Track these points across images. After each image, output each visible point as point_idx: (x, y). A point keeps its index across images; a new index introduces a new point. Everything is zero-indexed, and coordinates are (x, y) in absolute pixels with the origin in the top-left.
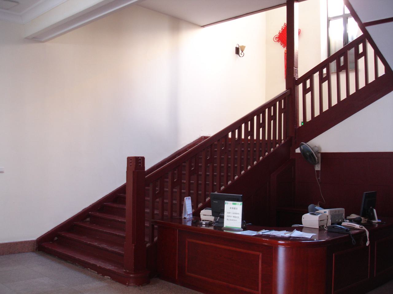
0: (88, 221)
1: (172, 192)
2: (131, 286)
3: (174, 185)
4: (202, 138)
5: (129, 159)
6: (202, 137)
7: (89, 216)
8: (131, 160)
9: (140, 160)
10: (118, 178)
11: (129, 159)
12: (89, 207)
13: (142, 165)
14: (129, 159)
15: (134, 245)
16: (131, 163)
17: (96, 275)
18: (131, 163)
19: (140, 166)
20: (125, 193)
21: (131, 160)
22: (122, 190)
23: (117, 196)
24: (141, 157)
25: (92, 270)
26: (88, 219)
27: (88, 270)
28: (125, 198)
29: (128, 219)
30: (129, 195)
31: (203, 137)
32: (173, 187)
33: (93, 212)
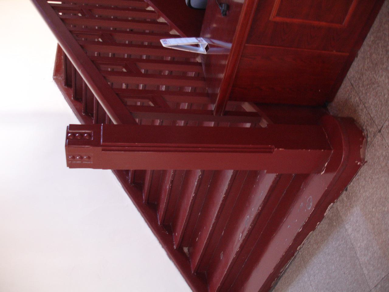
0: (189, 250)
1: (146, 75)
2: (364, 153)
3: (133, 71)
4: (56, 78)
5: (72, 163)
6: (54, 79)
7: (180, 248)
8: (74, 157)
9: (74, 134)
10: (103, 187)
11: (322, 249)
12: (173, 262)
13: (87, 131)
14: (72, 163)
15: (276, 149)
16: (81, 158)
17: (314, 233)
18: (81, 158)
19: (89, 135)
20: (127, 171)
21: (74, 157)
22: (122, 175)
23: (137, 186)
24: (68, 133)
25: (303, 243)
26: (186, 250)
27: (300, 249)
28: (135, 172)
29: (195, 166)
30: (144, 160)
31: (55, 77)
32: (139, 74)
33: (174, 243)
